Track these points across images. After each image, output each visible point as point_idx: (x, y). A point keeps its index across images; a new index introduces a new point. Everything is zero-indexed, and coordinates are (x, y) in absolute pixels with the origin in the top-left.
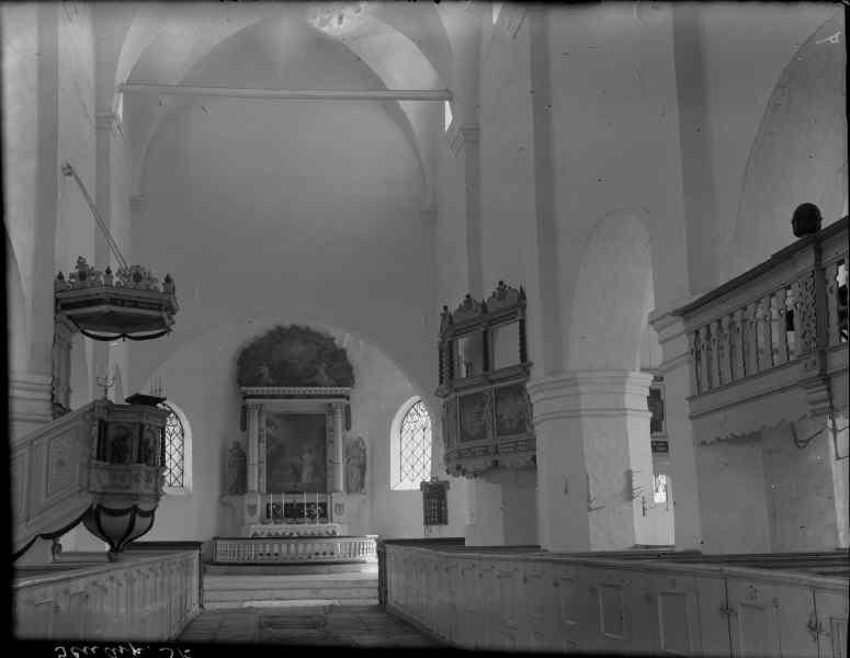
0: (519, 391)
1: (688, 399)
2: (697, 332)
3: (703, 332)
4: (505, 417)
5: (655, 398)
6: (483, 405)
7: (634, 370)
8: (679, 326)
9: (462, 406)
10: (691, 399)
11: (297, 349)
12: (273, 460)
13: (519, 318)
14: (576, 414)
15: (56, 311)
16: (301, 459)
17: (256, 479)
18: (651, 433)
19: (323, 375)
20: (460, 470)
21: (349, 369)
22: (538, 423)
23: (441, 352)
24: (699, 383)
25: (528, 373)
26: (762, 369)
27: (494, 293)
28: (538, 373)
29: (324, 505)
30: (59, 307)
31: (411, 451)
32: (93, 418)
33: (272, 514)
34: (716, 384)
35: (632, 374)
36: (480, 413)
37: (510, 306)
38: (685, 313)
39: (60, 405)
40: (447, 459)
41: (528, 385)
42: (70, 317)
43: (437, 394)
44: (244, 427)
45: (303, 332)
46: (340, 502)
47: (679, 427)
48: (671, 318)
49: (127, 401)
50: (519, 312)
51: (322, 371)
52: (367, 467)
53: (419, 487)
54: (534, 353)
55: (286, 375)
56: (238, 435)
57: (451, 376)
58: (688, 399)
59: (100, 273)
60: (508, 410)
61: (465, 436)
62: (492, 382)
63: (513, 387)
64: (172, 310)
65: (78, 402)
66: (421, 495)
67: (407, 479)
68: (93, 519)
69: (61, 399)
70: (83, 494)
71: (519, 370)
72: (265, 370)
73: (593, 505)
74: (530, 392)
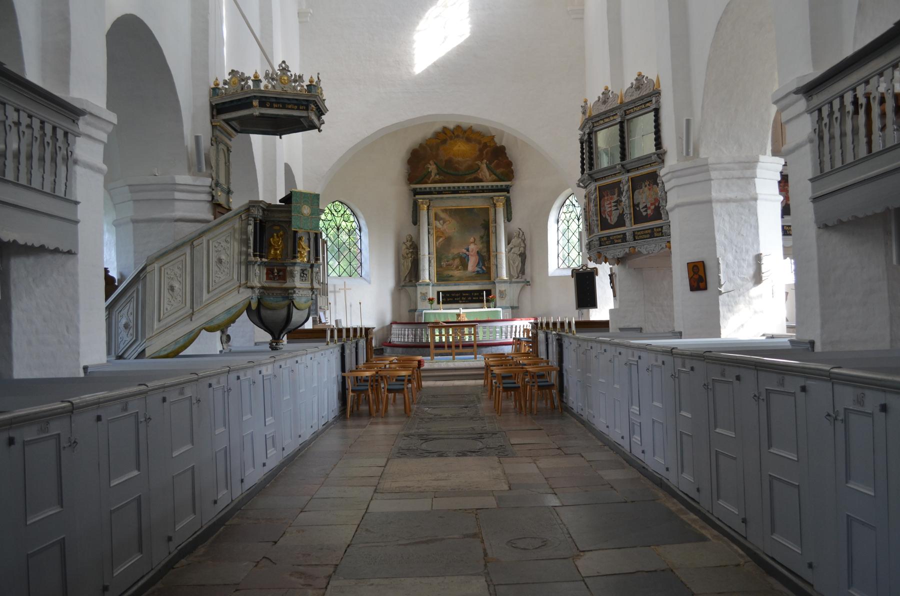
0: (653, 178)
1: (810, 180)
2: (820, 110)
3: (825, 111)
4: (641, 206)
5: (784, 182)
6: (620, 194)
7: (765, 154)
8: (802, 104)
9: (601, 197)
10: (812, 180)
11: (460, 149)
12: (440, 256)
13: (653, 107)
14: (710, 202)
15: (213, 117)
16: (468, 250)
17: (427, 272)
18: (782, 217)
19: (485, 172)
20: (600, 258)
21: (509, 164)
22: (672, 209)
23: (582, 143)
24: (821, 163)
25: (663, 161)
26: (888, 146)
27: (632, 84)
28: (672, 160)
29: (489, 292)
30: (215, 113)
31: (562, 241)
32: (248, 216)
33: (450, 298)
34: (838, 164)
35: (762, 158)
36: (618, 202)
37: (646, 99)
38: (809, 90)
39: (220, 205)
40: (589, 246)
41: (662, 172)
42: (227, 121)
43: (579, 186)
44: (416, 221)
45: (465, 132)
46: (503, 289)
47: (805, 211)
48: (795, 96)
49: (280, 201)
50: (654, 100)
51: (484, 166)
52: (527, 255)
53: (570, 274)
54: (669, 141)
55: (451, 171)
56: (410, 230)
57: (591, 166)
58: (810, 180)
59: (249, 78)
60: (644, 197)
61: (605, 224)
62: (628, 171)
63: (648, 177)
64: (320, 112)
65: (237, 203)
66: (572, 282)
67: (345, 274)
68: (258, 315)
69: (221, 198)
70: (242, 290)
71: (654, 158)
72: (432, 168)
73: (722, 289)
74: (664, 179)
